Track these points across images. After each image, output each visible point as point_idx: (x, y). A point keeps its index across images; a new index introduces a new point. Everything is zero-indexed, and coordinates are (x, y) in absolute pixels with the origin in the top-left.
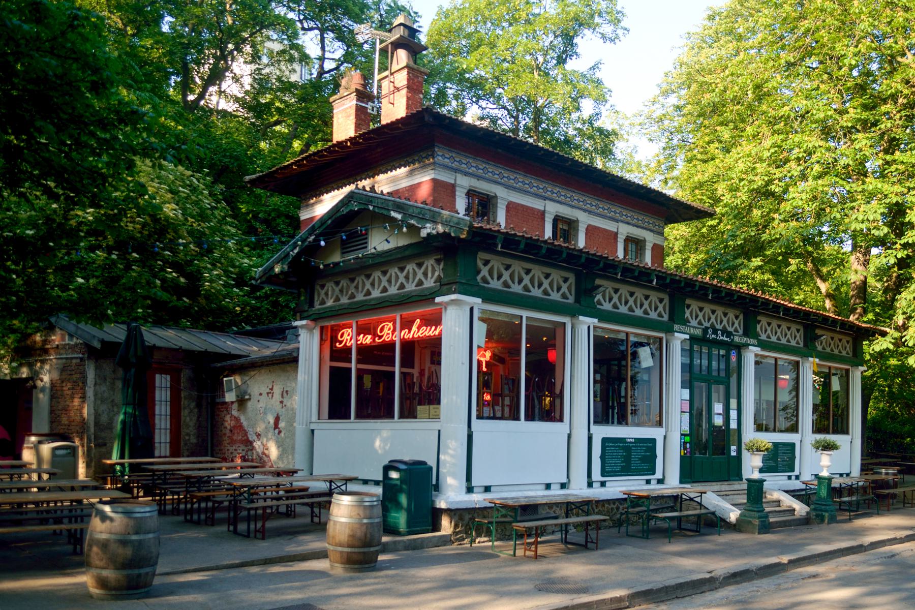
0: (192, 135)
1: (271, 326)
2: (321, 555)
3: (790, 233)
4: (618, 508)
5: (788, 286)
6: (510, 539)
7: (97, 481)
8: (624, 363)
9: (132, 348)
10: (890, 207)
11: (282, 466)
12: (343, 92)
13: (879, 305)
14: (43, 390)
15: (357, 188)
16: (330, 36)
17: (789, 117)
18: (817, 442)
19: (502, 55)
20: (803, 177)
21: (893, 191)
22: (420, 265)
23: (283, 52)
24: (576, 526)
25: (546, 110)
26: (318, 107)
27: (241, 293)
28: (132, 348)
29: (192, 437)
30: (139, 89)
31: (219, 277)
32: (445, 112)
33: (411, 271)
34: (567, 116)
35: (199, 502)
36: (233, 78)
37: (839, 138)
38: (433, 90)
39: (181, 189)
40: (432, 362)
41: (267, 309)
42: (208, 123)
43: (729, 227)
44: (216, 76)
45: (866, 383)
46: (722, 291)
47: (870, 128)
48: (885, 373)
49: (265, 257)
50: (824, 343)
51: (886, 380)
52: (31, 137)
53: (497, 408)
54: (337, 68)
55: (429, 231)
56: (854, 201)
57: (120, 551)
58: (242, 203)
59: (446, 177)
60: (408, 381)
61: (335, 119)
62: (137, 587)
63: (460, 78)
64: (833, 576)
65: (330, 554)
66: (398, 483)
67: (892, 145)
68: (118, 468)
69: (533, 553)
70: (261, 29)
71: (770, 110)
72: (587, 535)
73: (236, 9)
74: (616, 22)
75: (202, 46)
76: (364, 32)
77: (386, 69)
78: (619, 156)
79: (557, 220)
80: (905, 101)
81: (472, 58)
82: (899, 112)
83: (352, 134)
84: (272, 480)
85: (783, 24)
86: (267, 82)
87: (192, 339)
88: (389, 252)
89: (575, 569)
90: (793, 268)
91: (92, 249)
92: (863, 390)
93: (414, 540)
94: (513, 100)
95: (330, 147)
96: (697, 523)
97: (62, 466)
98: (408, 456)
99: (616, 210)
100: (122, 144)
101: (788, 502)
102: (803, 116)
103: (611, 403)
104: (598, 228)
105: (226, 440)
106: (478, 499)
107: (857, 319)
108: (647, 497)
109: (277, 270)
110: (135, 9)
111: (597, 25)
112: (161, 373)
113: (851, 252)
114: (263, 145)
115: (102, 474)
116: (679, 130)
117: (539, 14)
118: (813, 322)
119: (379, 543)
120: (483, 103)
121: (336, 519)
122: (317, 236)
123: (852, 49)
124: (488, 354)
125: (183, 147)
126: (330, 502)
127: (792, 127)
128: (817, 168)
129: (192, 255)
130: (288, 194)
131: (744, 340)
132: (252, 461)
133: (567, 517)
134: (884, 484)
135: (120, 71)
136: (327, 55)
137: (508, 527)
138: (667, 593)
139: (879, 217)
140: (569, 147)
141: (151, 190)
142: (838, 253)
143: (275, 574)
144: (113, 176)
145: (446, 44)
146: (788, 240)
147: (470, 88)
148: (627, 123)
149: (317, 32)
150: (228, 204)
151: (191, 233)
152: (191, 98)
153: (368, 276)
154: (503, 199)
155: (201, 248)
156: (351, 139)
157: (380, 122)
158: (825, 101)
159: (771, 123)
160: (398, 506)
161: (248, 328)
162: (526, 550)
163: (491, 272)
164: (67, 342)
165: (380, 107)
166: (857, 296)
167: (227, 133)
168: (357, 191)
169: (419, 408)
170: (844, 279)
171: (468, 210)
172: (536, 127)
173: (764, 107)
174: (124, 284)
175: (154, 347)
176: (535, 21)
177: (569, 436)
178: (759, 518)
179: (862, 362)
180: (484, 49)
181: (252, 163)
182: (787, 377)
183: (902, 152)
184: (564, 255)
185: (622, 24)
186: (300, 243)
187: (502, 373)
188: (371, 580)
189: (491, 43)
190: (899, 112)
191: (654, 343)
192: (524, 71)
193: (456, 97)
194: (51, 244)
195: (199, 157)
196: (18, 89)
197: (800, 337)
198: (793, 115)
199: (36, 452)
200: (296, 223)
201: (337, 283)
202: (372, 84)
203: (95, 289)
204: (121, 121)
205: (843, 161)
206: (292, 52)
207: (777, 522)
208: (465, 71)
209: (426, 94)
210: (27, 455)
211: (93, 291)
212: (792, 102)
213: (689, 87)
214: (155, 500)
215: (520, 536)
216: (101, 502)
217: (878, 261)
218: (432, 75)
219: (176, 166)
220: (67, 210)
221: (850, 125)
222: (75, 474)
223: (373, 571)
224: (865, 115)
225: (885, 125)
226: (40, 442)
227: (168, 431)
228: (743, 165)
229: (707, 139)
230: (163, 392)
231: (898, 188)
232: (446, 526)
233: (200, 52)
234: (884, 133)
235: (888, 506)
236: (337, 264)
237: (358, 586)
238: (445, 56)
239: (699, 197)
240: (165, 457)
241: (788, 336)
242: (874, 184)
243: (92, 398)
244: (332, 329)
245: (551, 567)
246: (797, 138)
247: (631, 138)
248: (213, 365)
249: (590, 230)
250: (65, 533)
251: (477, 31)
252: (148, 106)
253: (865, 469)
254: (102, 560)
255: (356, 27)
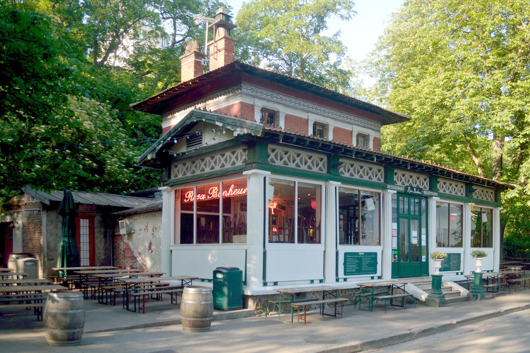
0: (100, 81)
1: (146, 190)
2: (178, 322)
3: (457, 129)
4: (354, 294)
5: (456, 161)
6: (289, 312)
7: (49, 280)
8: (357, 208)
9: (67, 205)
10: (515, 113)
11: (154, 271)
12: (187, 53)
13: (510, 171)
14: (18, 228)
15: (195, 108)
16: (179, 21)
17: (454, 61)
18: (474, 252)
19: (281, 29)
20: (464, 96)
21: (517, 104)
22: (233, 153)
23: (152, 32)
24: (329, 304)
25: (308, 60)
26: (172, 63)
27: (128, 172)
28: (67, 205)
29: (102, 255)
30: (70, 57)
31: (116, 162)
32: (248, 63)
33: (228, 156)
34: (321, 63)
35: (107, 292)
36: (123, 48)
37: (484, 73)
38: (240, 51)
39: (93, 112)
40: (242, 210)
41: (144, 180)
42: (109, 74)
43: (420, 126)
44: (113, 47)
45: (502, 217)
46: (416, 165)
47: (503, 67)
48: (514, 211)
49: (142, 150)
50: (477, 194)
51: (514, 215)
52: (11, 86)
53: (281, 236)
54: (183, 40)
55: (238, 132)
56: (494, 110)
57: (63, 319)
58: (129, 119)
59: (249, 101)
60: (227, 221)
61: (182, 69)
62: (73, 340)
63: (256, 43)
64: (482, 330)
65: (183, 322)
66: (222, 280)
67: (516, 77)
68: (61, 272)
69: (303, 321)
70: (139, 19)
71: (443, 57)
72: (336, 309)
73: (125, 9)
74: (349, 8)
75: (105, 30)
76: (199, 19)
77: (212, 39)
78: (352, 86)
79: (315, 125)
80: (522, 51)
81: (263, 31)
82: (519, 57)
83: (192, 77)
84: (149, 279)
85: (449, 7)
86: (143, 49)
87: (101, 199)
88: (215, 145)
89: (329, 329)
90: (458, 150)
91: (44, 148)
92: (501, 221)
93: (233, 313)
94: (288, 54)
95: (180, 85)
96: (402, 302)
97: (30, 272)
98: (228, 265)
99: (352, 118)
100: (60, 88)
101: (457, 288)
102: (462, 61)
103: (350, 232)
104: (341, 129)
105: (121, 257)
106: (270, 290)
107: (497, 179)
108: (372, 287)
109: (149, 157)
110: (68, 12)
111: (338, 10)
112: (83, 219)
113: (493, 140)
114: (140, 85)
115: (52, 276)
116: (388, 70)
117: (303, 5)
118: (471, 182)
119: (212, 315)
120: (270, 57)
121: (186, 302)
122: (172, 137)
123: (490, 21)
124: (275, 205)
125: (95, 88)
126: (182, 292)
127: (456, 67)
128: (472, 91)
129: (100, 150)
130: (155, 113)
131: (430, 193)
132: (136, 268)
133: (324, 299)
134: (513, 276)
135: (59, 47)
136: (178, 32)
137: (288, 305)
138: (384, 342)
139: (509, 119)
140: (322, 81)
141: (76, 114)
142: (485, 141)
143: (150, 333)
144: (55, 106)
145: (247, 24)
146: (455, 133)
147: (262, 49)
148: (357, 66)
149: (171, 19)
150: (120, 120)
151: (99, 138)
152: (99, 60)
153: (203, 160)
154: (283, 113)
155: (105, 146)
156: (192, 80)
157: (209, 70)
158: (475, 52)
159: (444, 64)
160: (222, 294)
161: (133, 192)
162: (299, 319)
163: (276, 156)
164: (31, 201)
165: (209, 61)
166: (497, 166)
167: (120, 80)
168: (195, 110)
169: (234, 236)
170: (489, 156)
171: (262, 119)
172: (302, 70)
173: (439, 56)
174: (62, 168)
175: (79, 204)
176: (300, 8)
177: (325, 252)
178: (439, 298)
179: (500, 205)
180: (270, 25)
181: (134, 96)
182: (456, 214)
183: (521, 81)
184: (320, 145)
185: (353, 9)
186: (162, 142)
187: (283, 215)
188: (207, 336)
189: (274, 22)
190: (519, 57)
191: (375, 196)
192: (295, 37)
193: (254, 54)
194: (22, 146)
195: (103, 94)
196: (4, 60)
197: (463, 190)
198: (456, 60)
199: (15, 263)
200: (159, 130)
201: (184, 164)
202: (204, 48)
203: (47, 172)
204: (60, 75)
205: (487, 87)
206: (157, 31)
207: (450, 300)
208: (259, 39)
209: (236, 53)
210: (11, 265)
211: (45, 172)
212: (456, 53)
213: (394, 45)
214: (81, 291)
215: (296, 311)
216: (52, 292)
217: (509, 145)
218: (239, 42)
219: (90, 99)
220: (30, 127)
221: (490, 65)
222: (37, 276)
223: (208, 331)
224: (499, 59)
225: (511, 65)
226: (17, 258)
227: (88, 251)
228: (427, 90)
229: (405, 75)
230: (85, 229)
231: (520, 102)
232: (251, 305)
233: (104, 34)
234: (511, 70)
235: (515, 289)
236: (184, 153)
237: (199, 340)
238: (247, 31)
239: (402, 109)
240: (87, 266)
241: (456, 190)
242: (506, 99)
243: (45, 233)
244: (182, 192)
245: (314, 328)
246: (459, 73)
247: (359, 75)
248: (112, 213)
249: (336, 130)
250: (33, 309)
251: (266, 16)
252: (75, 66)
253: (502, 267)
254: (53, 324)
255: (194, 16)
